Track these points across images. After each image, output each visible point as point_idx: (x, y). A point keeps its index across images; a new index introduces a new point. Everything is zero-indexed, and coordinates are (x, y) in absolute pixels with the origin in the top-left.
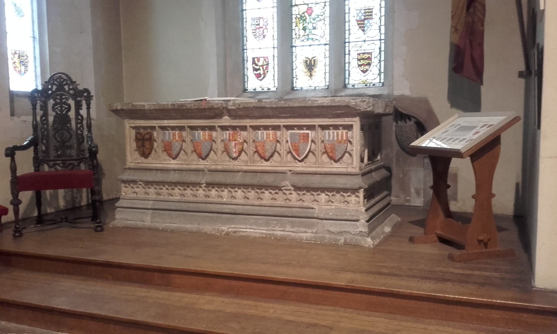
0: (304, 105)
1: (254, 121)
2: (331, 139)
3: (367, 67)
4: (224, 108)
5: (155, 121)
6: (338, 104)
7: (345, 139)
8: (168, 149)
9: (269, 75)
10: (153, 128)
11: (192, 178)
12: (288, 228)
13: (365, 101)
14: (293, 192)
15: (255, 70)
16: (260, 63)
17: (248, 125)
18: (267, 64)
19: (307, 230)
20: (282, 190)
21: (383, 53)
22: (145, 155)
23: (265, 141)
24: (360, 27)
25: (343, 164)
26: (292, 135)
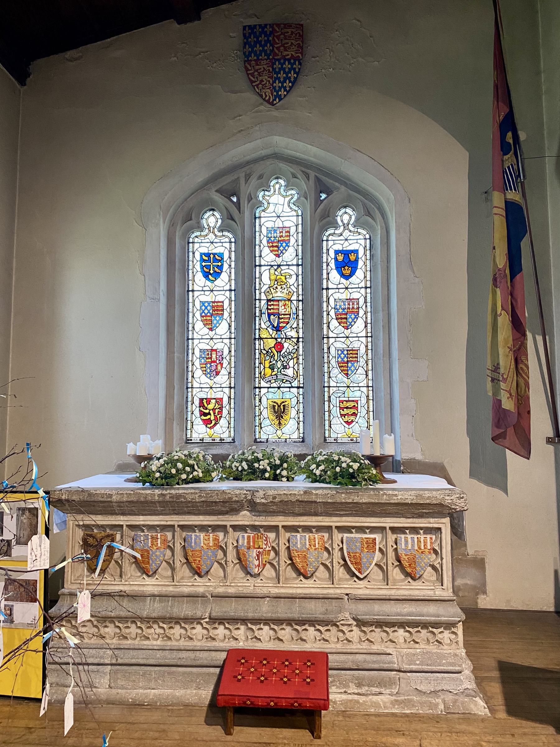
0: (376, 501)
1: (290, 518)
3: (352, 418)
5: (122, 518)
6: (428, 501)
9: (223, 422)
11: (186, 610)
12: (353, 688)
13: (462, 498)
14: (354, 628)
16: (211, 406)
18: (221, 408)
19: (382, 690)
20: (338, 626)
23: (308, 549)
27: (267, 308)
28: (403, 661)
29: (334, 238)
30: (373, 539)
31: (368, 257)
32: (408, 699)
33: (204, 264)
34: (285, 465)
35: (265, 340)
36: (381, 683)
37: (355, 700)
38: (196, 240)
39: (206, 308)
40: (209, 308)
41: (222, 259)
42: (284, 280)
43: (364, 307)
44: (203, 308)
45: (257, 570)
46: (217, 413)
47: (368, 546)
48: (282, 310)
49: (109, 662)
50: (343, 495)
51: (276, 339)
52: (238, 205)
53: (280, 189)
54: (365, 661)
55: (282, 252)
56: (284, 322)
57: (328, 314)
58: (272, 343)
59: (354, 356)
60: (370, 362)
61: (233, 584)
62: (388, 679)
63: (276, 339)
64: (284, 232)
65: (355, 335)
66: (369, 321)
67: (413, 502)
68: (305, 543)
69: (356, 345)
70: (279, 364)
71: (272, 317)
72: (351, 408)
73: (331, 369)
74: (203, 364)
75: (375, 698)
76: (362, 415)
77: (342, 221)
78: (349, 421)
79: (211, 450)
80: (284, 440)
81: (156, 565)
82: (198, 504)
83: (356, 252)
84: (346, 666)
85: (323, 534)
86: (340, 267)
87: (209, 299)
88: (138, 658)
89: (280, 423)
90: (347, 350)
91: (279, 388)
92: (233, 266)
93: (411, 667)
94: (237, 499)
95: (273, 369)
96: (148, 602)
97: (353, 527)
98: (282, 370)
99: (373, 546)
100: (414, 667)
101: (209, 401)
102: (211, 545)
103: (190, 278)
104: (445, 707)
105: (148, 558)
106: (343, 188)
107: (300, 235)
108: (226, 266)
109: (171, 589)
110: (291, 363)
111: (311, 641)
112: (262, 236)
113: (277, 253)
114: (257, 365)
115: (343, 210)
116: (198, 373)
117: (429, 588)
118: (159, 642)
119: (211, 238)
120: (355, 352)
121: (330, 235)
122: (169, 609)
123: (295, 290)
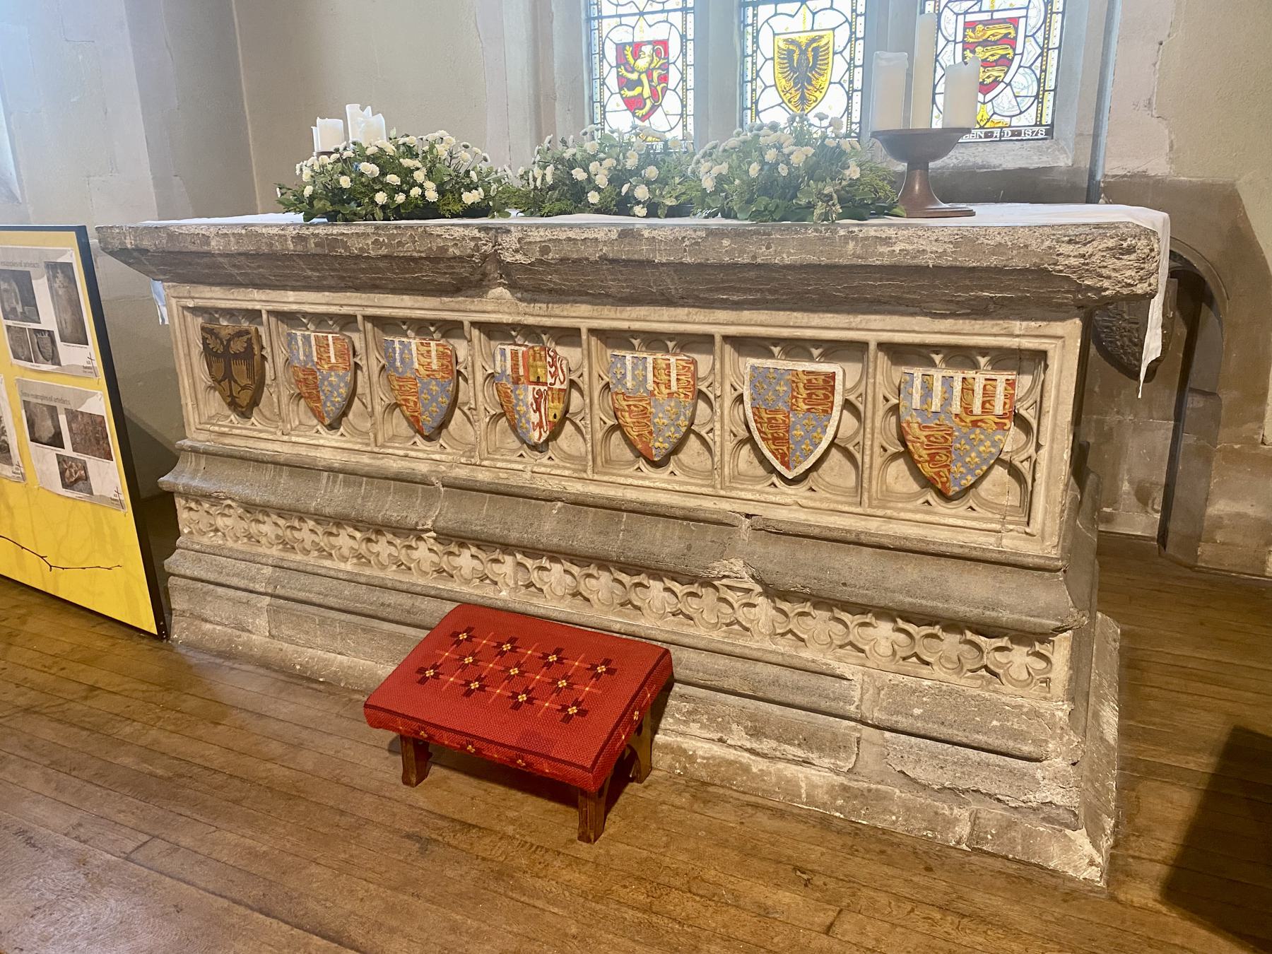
0: (824, 260)
1: (607, 311)
2: (936, 404)
4: (485, 257)
5: (256, 294)
6: (994, 261)
7: (999, 410)
8: (308, 389)
9: (671, 102)
10: (254, 315)
11: (391, 507)
12: (738, 736)
13: (1131, 250)
15: (624, 83)
16: (642, 64)
17: (584, 325)
18: (665, 67)
19: (813, 756)
21: (690, 46)
22: (244, 406)
23: (652, 394)
25: (981, 512)
26: (759, 378)
28: (875, 702)
32: (877, 790)
36: (809, 741)
37: (741, 764)
45: (536, 434)
47: (810, 395)
49: (262, 590)
50: (726, 242)
54: (775, 682)
61: (486, 463)
62: (829, 736)
67: (943, 262)
68: (645, 376)
72: (995, 43)
75: (791, 770)
76: (1026, 62)
81: (333, 403)
82: (381, 265)
84: (726, 685)
88: (310, 592)
89: (803, 99)
93: (894, 718)
94: (458, 253)
96: (324, 482)
97: (777, 341)
99: (826, 397)
100: (903, 722)
101: (637, 48)
102: (435, 367)
104: (971, 834)
105: (316, 387)
109: (366, 459)
111: (654, 612)
117: (984, 526)
118: (348, 567)
122: (359, 501)
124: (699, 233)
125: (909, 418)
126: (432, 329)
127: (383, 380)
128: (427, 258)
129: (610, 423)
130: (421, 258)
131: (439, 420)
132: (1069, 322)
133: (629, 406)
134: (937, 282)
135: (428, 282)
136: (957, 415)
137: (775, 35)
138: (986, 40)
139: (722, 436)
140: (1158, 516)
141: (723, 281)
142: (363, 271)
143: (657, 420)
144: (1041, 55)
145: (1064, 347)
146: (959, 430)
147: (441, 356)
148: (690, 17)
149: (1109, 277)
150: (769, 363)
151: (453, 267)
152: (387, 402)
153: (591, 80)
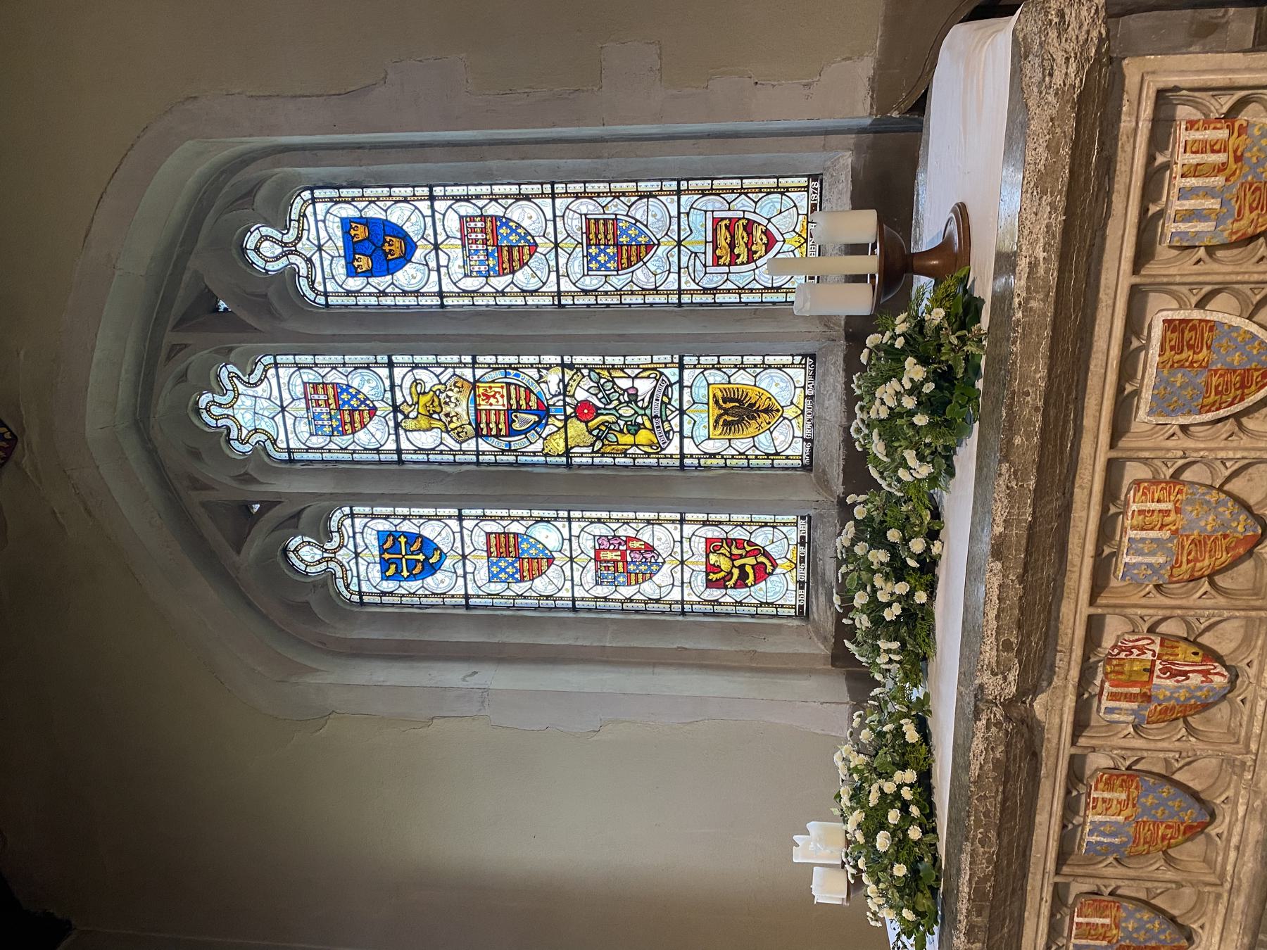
0: (1047, 333)
1: (1070, 583)
2: (1212, 204)
3: (758, 233)
4: (1008, 718)
6: (1065, 151)
7: (1223, 134)
13: (1061, 14)
15: (742, 582)
16: (725, 564)
17: (1085, 610)
18: (729, 542)
21: (713, 517)
23: (1175, 532)
24: (640, 259)
27: (497, 436)
29: (319, 278)
30: (1165, 331)
31: (356, 192)
33: (405, 574)
34: (893, 535)
35: (571, 443)
38: (354, 587)
39: (503, 570)
40: (502, 564)
41: (390, 533)
42: (428, 397)
43: (480, 203)
44: (503, 576)
45: (1217, 679)
46: (740, 552)
47: (1190, 347)
48: (499, 403)
51: (567, 418)
52: (267, 506)
53: (220, 405)
55: (363, 402)
56: (528, 400)
57: (503, 294)
58: (576, 427)
59: (602, 228)
60: (617, 187)
63: (567, 418)
64: (316, 397)
65: (550, 225)
66: (514, 189)
67: (1062, 205)
68: (1152, 540)
69: (575, 223)
70: (626, 412)
71: (516, 426)
72: (733, 237)
73: (635, 288)
74: (629, 579)
77: (277, 258)
78: (765, 240)
79: (827, 573)
80: (808, 403)
81: (1164, 931)
82: (1005, 841)
83: (347, 224)
85: (1127, 482)
86: (386, 265)
87: (482, 564)
89: (768, 411)
90: (589, 245)
91: (682, 412)
92: (405, 511)
94: (1001, 748)
95: (639, 427)
98: (640, 404)
99: (1193, 328)
101: (711, 568)
102: (1123, 796)
103: (440, 601)
106: (193, 263)
107: (320, 359)
108: (407, 527)
109: (1239, 902)
110: (624, 383)
112: (332, 446)
113: (366, 414)
114: (628, 461)
115: (252, 255)
116: (649, 589)
119: (352, 553)
120: (592, 226)
121: (313, 288)
123: (450, 371)
124: (1004, 471)
125: (1226, 234)
126: (1075, 793)
127: (1133, 863)
128: (1005, 784)
129: (1206, 587)
130: (1003, 792)
131: (1191, 801)
132: (1126, 71)
133: (1188, 562)
134: (1079, 211)
135: (1025, 789)
136: (1227, 180)
137: (709, 438)
138: (730, 245)
139: (1235, 449)
140: (1232, 10)
141: (1055, 446)
142: (1009, 865)
143: (1209, 528)
144: (746, 194)
145: (1153, 73)
146: (1246, 176)
147: (1109, 786)
148: (689, 516)
149: (1088, 32)
150: (1147, 395)
151: (1015, 756)
152: (1163, 862)
153: (737, 615)
